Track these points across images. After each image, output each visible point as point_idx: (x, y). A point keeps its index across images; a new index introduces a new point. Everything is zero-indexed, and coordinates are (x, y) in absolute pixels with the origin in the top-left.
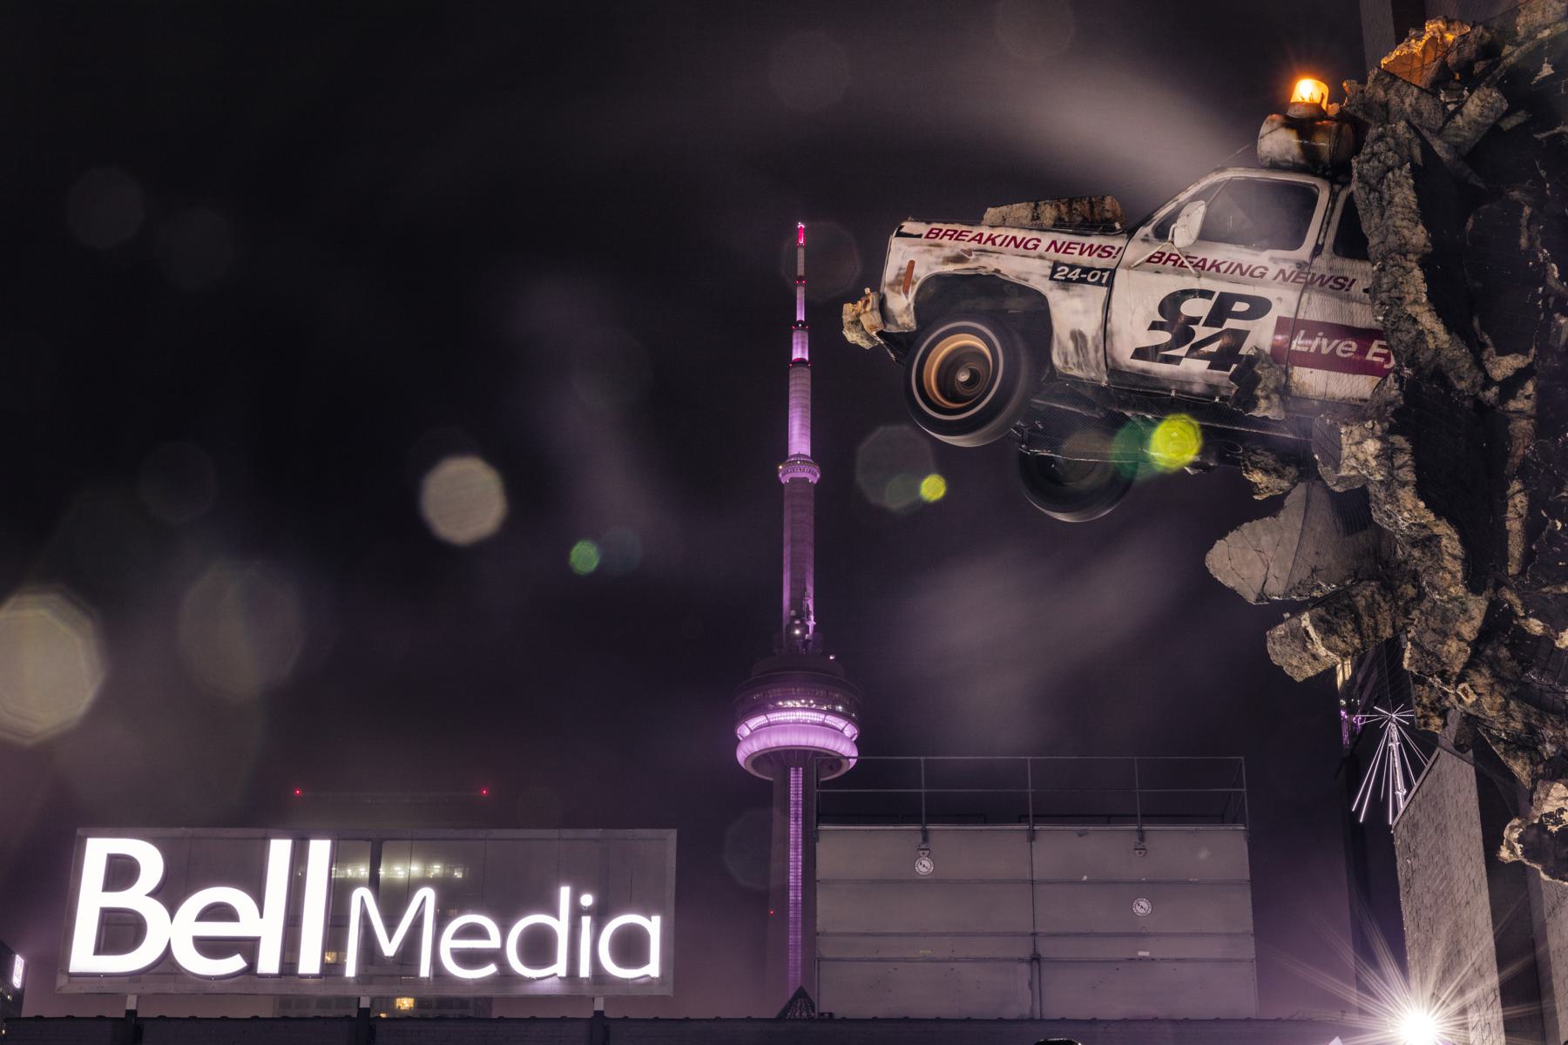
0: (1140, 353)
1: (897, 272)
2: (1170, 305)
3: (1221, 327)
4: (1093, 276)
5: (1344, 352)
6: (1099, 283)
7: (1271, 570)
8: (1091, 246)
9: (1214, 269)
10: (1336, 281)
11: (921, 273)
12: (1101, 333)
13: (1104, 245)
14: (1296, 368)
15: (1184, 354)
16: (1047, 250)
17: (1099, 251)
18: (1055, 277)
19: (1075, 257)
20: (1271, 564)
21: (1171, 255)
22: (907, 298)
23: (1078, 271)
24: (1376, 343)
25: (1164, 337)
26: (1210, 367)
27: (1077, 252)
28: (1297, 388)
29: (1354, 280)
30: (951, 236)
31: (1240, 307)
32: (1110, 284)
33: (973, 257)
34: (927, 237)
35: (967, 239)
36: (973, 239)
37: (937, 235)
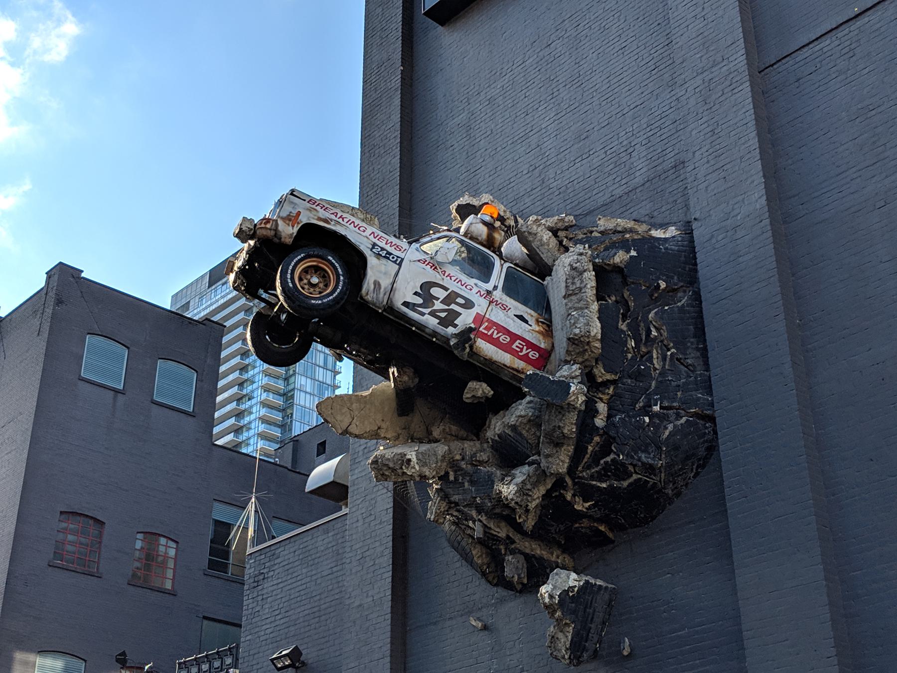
0: (406, 304)
2: (427, 286)
3: (449, 306)
4: (393, 258)
6: (395, 262)
7: (354, 421)
8: (392, 242)
11: (304, 219)
12: (390, 287)
13: (398, 244)
14: (479, 339)
15: (427, 313)
16: (370, 235)
19: (382, 244)
20: (355, 418)
22: (293, 229)
24: (518, 341)
25: (419, 301)
26: (438, 324)
27: (384, 242)
29: (510, 308)
30: (322, 208)
31: (462, 301)
32: (400, 265)
33: (332, 223)
34: (308, 202)
35: (330, 212)
36: (333, 214)
37: (314, 204)
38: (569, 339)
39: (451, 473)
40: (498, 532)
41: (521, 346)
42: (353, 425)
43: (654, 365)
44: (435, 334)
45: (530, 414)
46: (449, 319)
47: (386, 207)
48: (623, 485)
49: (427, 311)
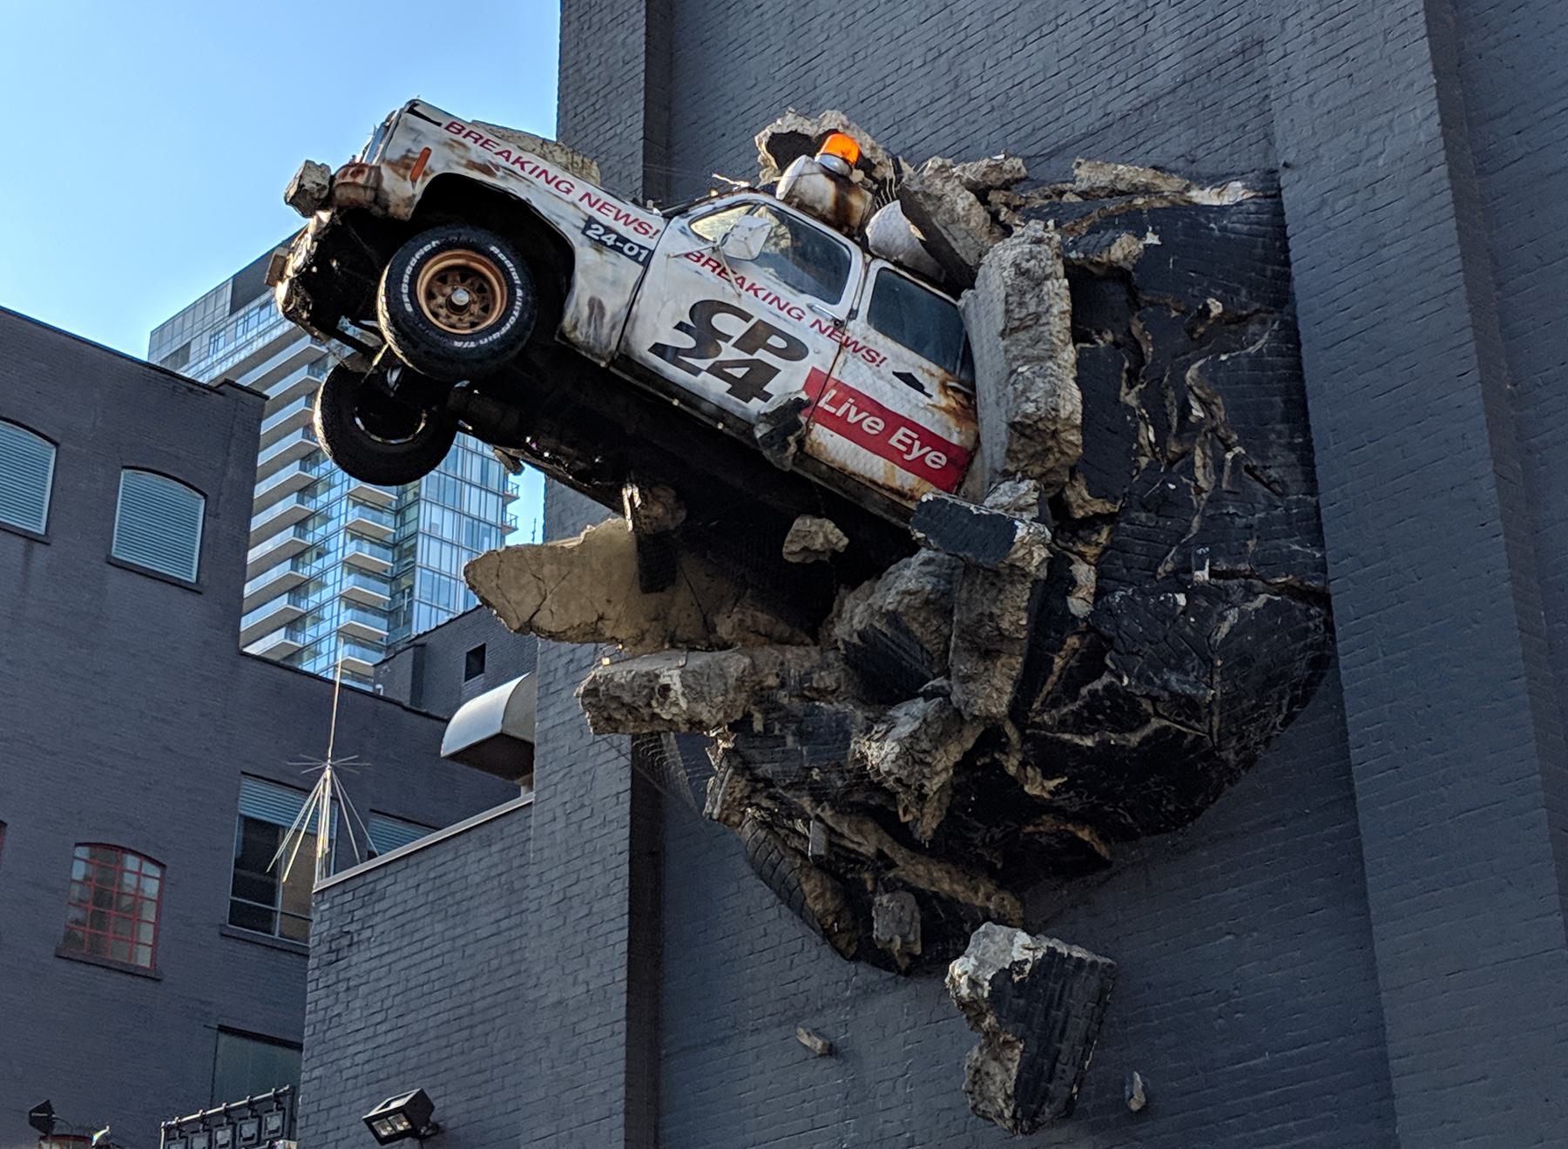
0: (659, 349)
1: (404, 153)
2: (704, 311)
5: (870, 427)
6: (635, 258)
7: (547, 602)
8: (628, 216)
9: (752, 292)
10: (868, 352)
12: (624, 312)
13: (641, 220)
14: (818, 425)
15: (705, 368)
16: (581, 200)
17: (635, 224)
18: (589, 233)
20: (549, 597)
21: (710, 259)
22: (414, 187)
23: (614, 237)
24: (903, 430)
25: (688, 342)
26: (728, 392)
27: (612, 215)
28: (811, 446)
30: (476, 141)
31: (775, 341)
33: (500, 174)
34: (447, 128)
38: (1012, 425)
39: (757, 716)
40: (860, 844)
41: (909, 441)
42: (544, 613)
43: (1196, 481)
44: (721, 413)
45: (929, 587)
46: (753, 382)
47: (616, 140)
48: (1129, 741)
49: (704, 364)
